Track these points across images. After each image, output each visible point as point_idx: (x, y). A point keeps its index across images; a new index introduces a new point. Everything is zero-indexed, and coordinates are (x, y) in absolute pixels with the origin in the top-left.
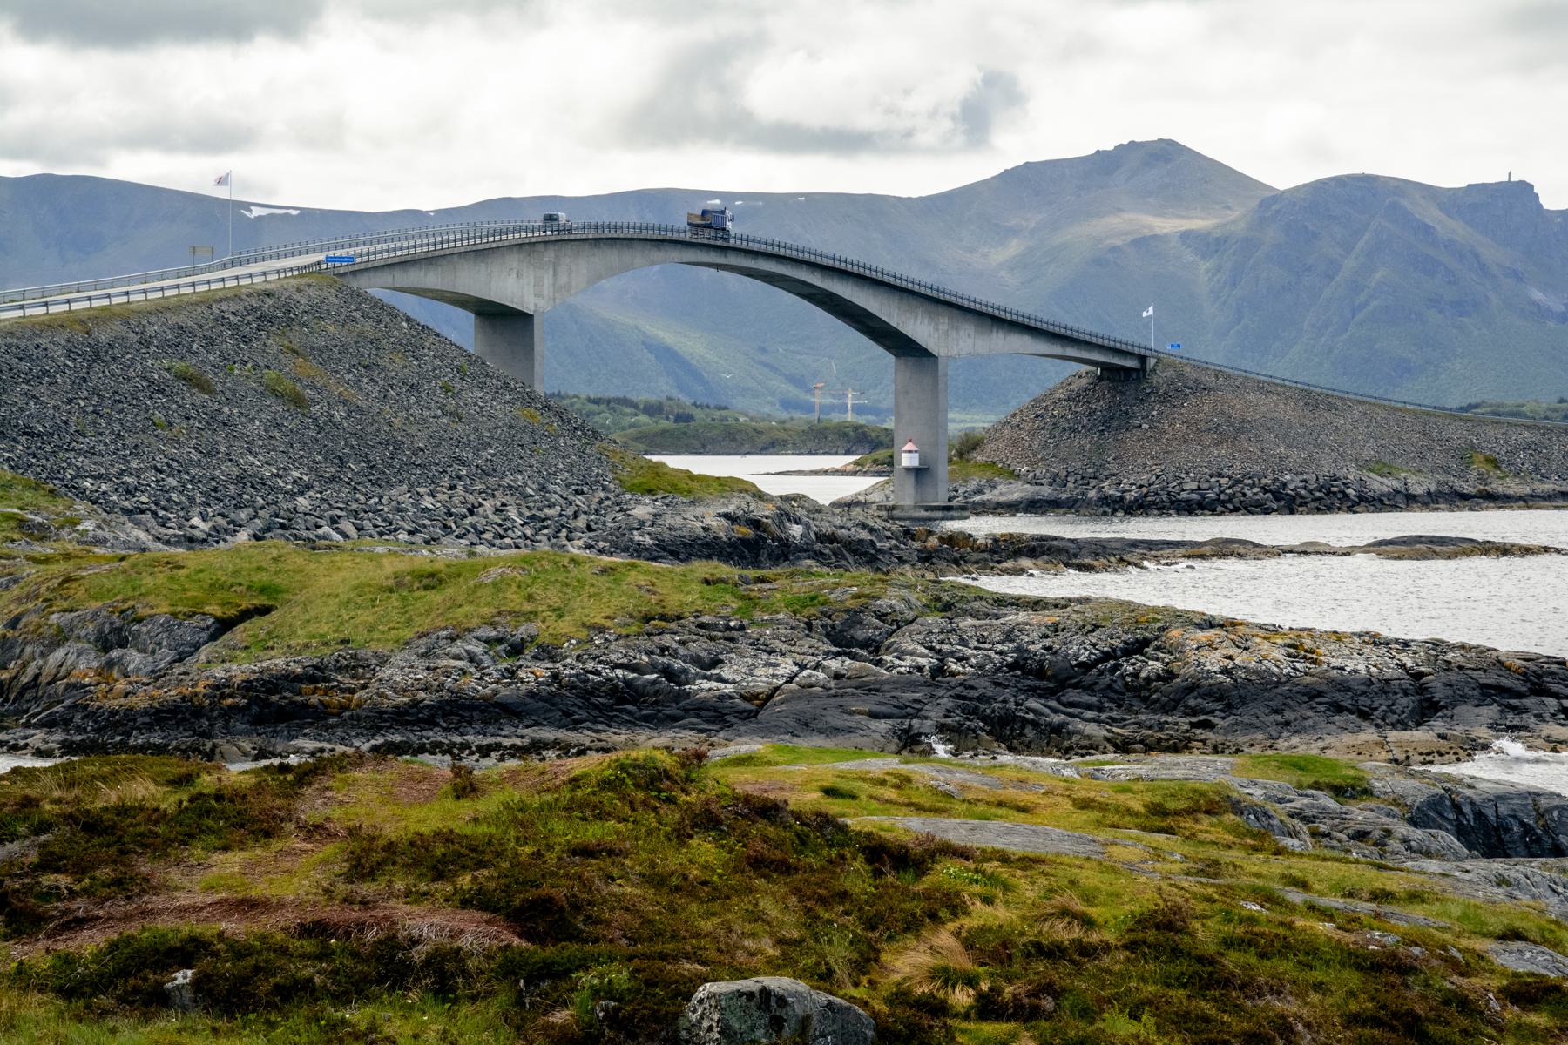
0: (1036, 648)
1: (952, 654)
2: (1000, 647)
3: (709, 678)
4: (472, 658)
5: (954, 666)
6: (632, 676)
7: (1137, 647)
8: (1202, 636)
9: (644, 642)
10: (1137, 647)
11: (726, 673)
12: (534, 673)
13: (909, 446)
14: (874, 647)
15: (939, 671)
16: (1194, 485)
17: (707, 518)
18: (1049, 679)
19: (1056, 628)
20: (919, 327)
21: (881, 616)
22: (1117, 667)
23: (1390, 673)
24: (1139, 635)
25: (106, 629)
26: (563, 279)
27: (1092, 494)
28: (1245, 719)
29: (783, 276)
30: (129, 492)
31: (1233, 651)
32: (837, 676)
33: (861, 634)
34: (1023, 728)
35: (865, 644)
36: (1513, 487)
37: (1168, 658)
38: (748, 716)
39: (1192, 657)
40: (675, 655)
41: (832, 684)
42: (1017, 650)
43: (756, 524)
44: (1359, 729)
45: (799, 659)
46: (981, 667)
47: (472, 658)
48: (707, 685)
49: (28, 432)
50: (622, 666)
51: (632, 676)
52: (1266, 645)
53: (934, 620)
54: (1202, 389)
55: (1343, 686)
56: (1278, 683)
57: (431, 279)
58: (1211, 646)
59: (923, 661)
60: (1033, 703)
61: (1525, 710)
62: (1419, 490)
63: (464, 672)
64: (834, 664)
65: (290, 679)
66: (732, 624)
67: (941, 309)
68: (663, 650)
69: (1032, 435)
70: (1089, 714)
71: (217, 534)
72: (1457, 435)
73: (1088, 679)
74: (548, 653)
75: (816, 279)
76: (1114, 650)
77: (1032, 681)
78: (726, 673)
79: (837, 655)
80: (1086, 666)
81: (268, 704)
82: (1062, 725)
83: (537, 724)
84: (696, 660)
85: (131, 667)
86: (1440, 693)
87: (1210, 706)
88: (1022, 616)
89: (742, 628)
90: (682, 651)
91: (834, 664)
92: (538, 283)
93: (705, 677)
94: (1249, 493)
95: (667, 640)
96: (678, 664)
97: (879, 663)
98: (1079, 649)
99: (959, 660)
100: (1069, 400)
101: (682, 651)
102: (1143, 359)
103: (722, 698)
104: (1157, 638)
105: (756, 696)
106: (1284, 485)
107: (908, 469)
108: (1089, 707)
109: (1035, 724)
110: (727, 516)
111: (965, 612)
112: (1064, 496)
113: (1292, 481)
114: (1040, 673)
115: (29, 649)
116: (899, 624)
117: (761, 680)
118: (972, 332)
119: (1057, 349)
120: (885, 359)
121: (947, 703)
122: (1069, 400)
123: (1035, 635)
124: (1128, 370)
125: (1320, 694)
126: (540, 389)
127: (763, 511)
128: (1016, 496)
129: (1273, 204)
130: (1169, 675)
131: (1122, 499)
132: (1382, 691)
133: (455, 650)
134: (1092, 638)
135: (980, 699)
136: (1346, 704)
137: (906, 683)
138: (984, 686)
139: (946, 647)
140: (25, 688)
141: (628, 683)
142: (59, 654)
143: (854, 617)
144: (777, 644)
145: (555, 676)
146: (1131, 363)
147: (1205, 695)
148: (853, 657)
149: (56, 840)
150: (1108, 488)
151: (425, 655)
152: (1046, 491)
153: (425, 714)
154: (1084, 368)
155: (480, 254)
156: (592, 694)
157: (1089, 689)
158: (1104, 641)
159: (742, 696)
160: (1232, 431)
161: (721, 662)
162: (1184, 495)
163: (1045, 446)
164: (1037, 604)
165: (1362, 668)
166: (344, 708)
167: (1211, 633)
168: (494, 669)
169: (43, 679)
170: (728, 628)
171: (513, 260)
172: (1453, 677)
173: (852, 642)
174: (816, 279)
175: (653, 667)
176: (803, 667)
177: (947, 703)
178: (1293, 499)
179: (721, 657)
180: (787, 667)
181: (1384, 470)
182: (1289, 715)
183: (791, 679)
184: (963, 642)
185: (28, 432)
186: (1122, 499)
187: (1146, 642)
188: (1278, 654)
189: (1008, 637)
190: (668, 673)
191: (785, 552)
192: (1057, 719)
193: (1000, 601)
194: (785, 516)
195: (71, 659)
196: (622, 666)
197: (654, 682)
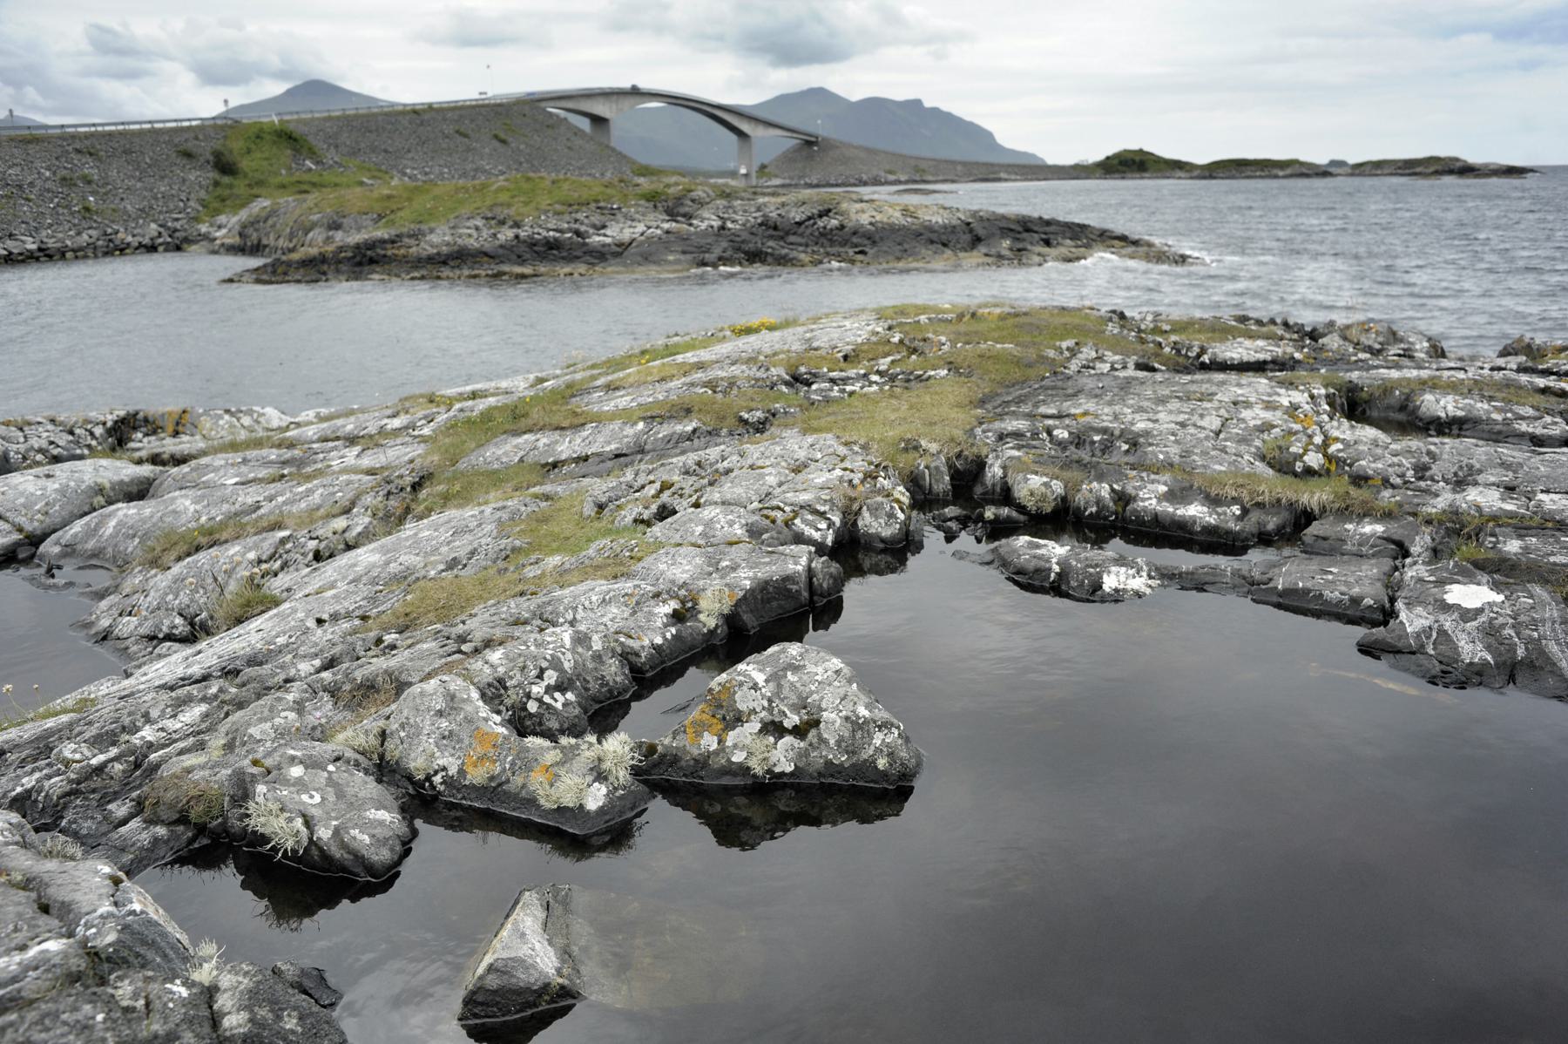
0: (774, 215)
1: (729, 219)
4: (477, 228)
5: (729, 225)
7: (825, 213)
8: (858, 206)
9: (567, 217)
10: (825, 213)
11: (608, 232)
12: (507, 234)
14: (689, 217)
15: (723, 228)
19: (783, 205)
20: (745, 127)
21: (693, 201)
22: (815, 223)
23: (955, 222)
24: (826, 207)
28: (885, 248)
30: (426, 174)
31: (874, 213)
32: (668, 232)
33: (682, 210)
35: (684, 215)
38: (617, 255)
39: (853, 217)
40: (582, 224)
41: (664, 236)
42: (763, 216)
44: (943, 252)
45: (649, 224)
46: (744, 225)
47: (477, 228)
48: (597, 239)
49: (386, 151)
52: (890, 210)
53: (721, 203)
55: (930, 229)
57: (570, 105)
58: (863, 211)
59: (714, 223)
60: (771, 243)
61: (1024, 240)
63: (470, 236)
64: (666, 226)
65: (383, 242)
68: (576, 221)
70: (801, 248)
77: (771, 232)
80: (799, 224)
81: (365, 256)
82: (786, 255)
83: (502, 262)
84: (594, 226)
86: (981, 232)
88: (766, 199)
89: (619, 209)
90: (586, 221)
91: (666, 226)
96: (583, 228)
97: (691, 225)
101: (586, 221)
103: (604, 245)
108: (801, 245)
109: (772, 255)
111: (737, 198)
113: (865, 177)
114: (775, 228)
116: (701, 203)
117: (626, 235)
119: (789, 134)
120: (733, 137)
121: (725, 244)
123: (772, 208)
125: (921, 234)
126: (613, 144)
130: (842, 227)
132: (953, 232)
133: (468, 224)
134: (802, 209)
135: (743, 242)
136: (935, 239)
137: (705, 234)
138: (745, 235)
139: (726, 216)
141: (556, 239)
143: (679, 200)
144: (637, 216)
145: (517, 237)
146: (813, 139)
148: (677, 221)
150: (808, 180)
151: (453, 228)
152: (787, 181)
153: (443, 258)
156: (535, 245)
157: (802, 235)
165: (940, 221)
166: (404, 256)
167: (863, 205)
168: (485, 233)
171: (601, 100)
172: (986, 224)
173: (678, 214)
175: (570, 230)
176: (649, 228)
177: (725, 244)
180: (641, 228)
181: (890, 172)
182: (906, 246)
183: (642, 234)
184: (735, 212)
185: (386, 151)
187: (830, 210)
188: (898, 214)
189: (759, 209)
190: (578, 233)
192: (784, 251)
197: (570, 238)
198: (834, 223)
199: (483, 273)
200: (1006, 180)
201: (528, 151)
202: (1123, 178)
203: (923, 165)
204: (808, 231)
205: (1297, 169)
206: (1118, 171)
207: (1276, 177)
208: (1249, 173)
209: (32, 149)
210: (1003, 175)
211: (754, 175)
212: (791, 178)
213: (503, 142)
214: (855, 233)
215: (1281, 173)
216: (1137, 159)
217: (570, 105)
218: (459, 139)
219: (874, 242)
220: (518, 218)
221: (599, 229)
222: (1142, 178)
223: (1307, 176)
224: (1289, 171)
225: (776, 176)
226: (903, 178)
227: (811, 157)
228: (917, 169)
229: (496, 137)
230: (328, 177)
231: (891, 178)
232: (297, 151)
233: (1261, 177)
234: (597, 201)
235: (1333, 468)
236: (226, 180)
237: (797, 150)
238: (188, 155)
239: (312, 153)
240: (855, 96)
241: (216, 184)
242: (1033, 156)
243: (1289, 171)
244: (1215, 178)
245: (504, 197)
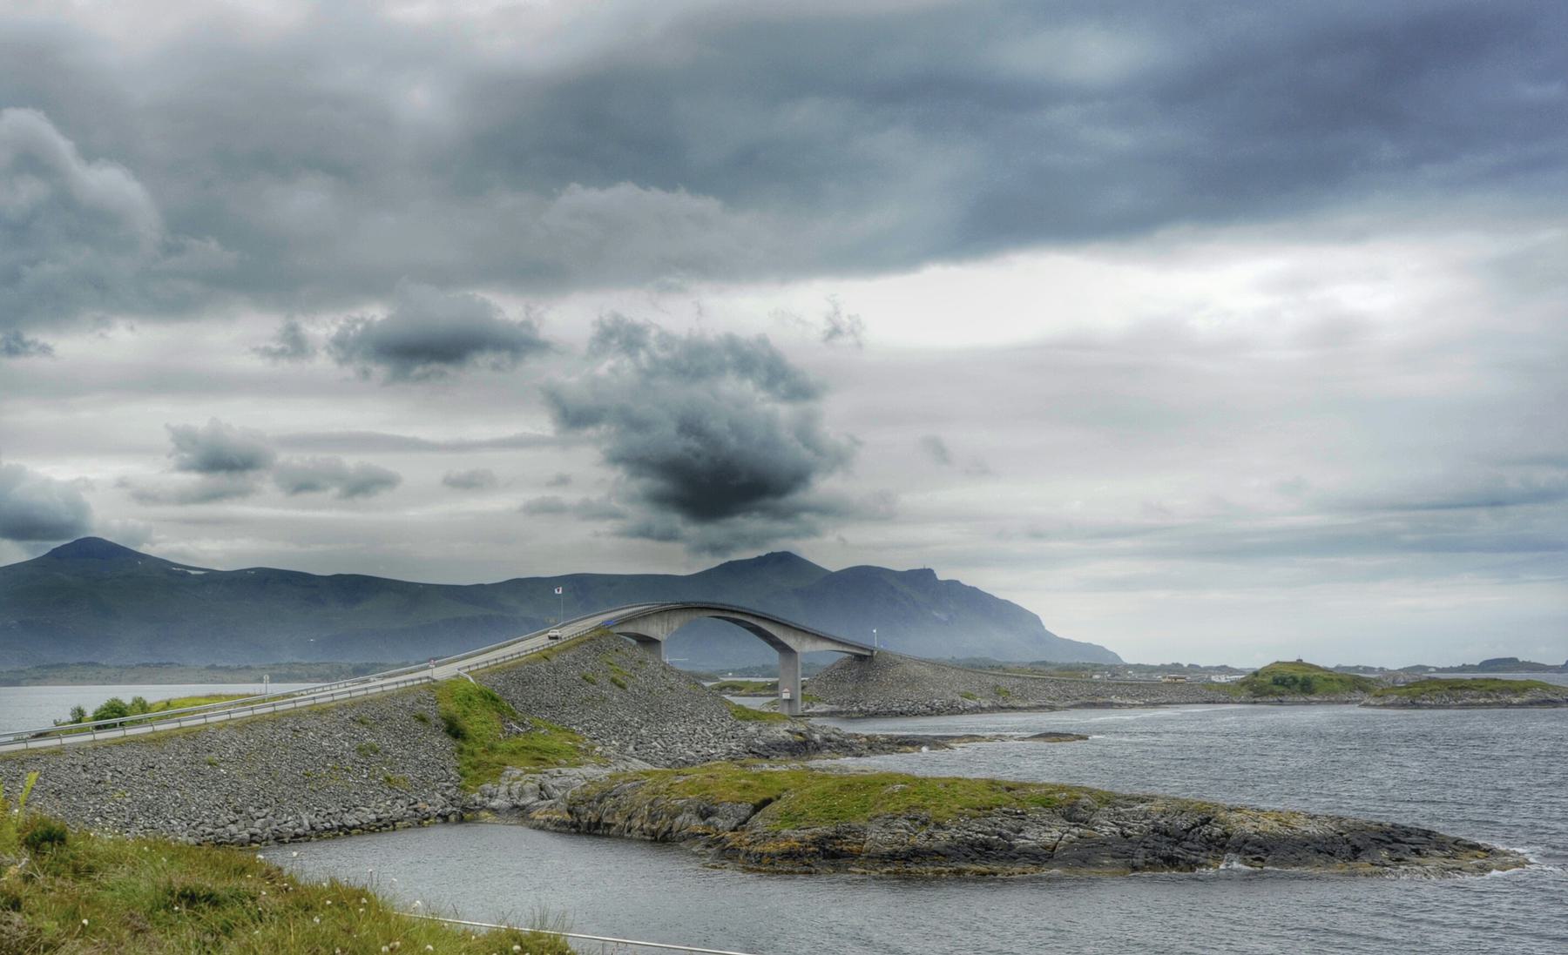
1: (1125, 825)
2: (1144, 822)
3: (1022, 838)
6: (986, 837)
13: (786, 690)
16: (897, 705)
18: (1170, 837)
22: (1200, 831)
25: (701, 808)
26: (670, 626)
27: (855, 708)
29: (743, 621)
34: (1177, 862)
37: (1222, 827)
42: (1153, 823)
43: (801, 734)
50: (980, 832)
51: (986, 837)
55: (1312, 839)
56: (1285, 840)
62: (986, 706)
66: (1019, 811)
67: (799, 633)
69: (827, 683)
73: (1190, 836)
76: (1196, 823)
78: (1029, 836)
79: (1074, 826)
80: (1187, 831)
85: (720, 826)
87: (1259, 850)
92: (663, 628)
93: (1019, 837)
94: (921, 708)
95: (994, 819)
98: (1182, 823)
99: (1129, 828)
100: (841, 668)
102: (872, 651)
104: (1214, 817)
105: (1048, 847)
106: (934, 704)
107: (785, 700)
109: (1183, 860)
110: (788, 731)
112: (844, 710)
115: (664, 816)
118: (809, 641)
122: (841, 668)
124: (865, 656)
128: (824, 710)
131: (868, 711)
140: (666, 833)
141: (986, 840)
142: (680, 819)
144: (1044, 821)
146: (867, 653)
147: (1254, 845)
152: (836, 707)
154: (847, 655)
159: (1042, 847)
160: (912, 681)
161: (1022, 830)
162: (894, 709)
163: (833, 689)
169: (674, 830)
170: (1017, 814)
171: (655, 619)
178: (938, 710)
179: (1023, 828)
180: (1056, 833)
186: (868, 711)
195: (687, 821)
196: (980, 832)
197: (997, 840)
198: (1217, 831)
199: (947, 870)
204: (1197, 838)
205: (1538, 694)
207: (1509, 705)
208: (1468, 700)
213: (622, 686)
214: (1245, 842)
215: (1516, 700)
216: (1300, 675)
219: (1266, 850)
220: (939, 820)
221: (1018, 833)
222: (1309, 703)
223: (1554, 703)
224: (1526, 698)
227: (862, 677)
229: (613, 681)
231: (970, 703)
234: (1000, 806)
241: (461, 751)
242: (1116, 656)
243: (1526, 698)
244: (1419, 706)
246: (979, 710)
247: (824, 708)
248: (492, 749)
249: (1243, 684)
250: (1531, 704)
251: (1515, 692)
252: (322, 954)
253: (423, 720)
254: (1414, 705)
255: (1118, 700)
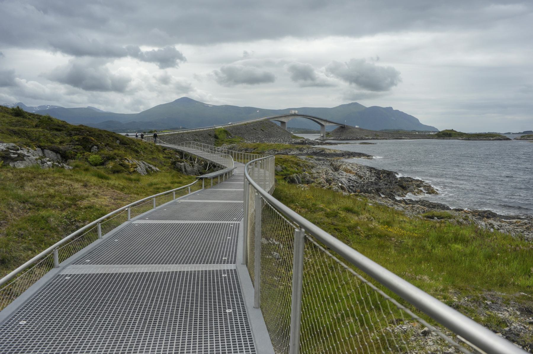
7: (323, 151)
14: (302, 151)
17: (299, 141)
20: (323, 123)
36: (379, 138)
54: (350, 128)
57: (276, 119)
71: (256, 142)
72: (375, 133)
74: (278, 151)
75: (313, 118)
116: (304, 149)
120: (320, 126)
127: (304, 140)
129: (440, 132)
149: (46, 163)
155: (281, 117)
158: (320, 151)
164: (316, 148)
174: (313, 118)
191: (306, 144)
193: (313, 148)
194: (306, 140)
200: (404, 139)
201: (338, 182)
202: (444, 139)
203: (378, 134)
205: (498, 137)
206: (442, 137)
207: (490, 140)
209: (189, 134)
210: (403, 137)
211: (325, 136)
212: (336, 137)
213: (263, 131)
217: (276, 119)
218: (254, 130)
222: (450, 139)
223: (500, 140)
224: (495, 138)
225: (332, 136)
226: (370, 138)
228: (376, 135)
229: (261, 129)
230: (233, 140)
231: (367, 138)
232: (227, 134)
233: (485, 140)
235: (382, 183)
236: (217, 140)
237: (339, 129)
238: (210, 135)
239: (230, 135)
240: (368, 106)
241: (216, 141)
243: (495, 138)
245: (275, 147)
246: (369, 139)
247: (332, 138)
248: (223, 141)
249: (436, 134)
250: (495, 140)
251: (492, 137)
252: (532, 246)
253: (210, 135)
254: (469, 140)
255: (404, 138)
